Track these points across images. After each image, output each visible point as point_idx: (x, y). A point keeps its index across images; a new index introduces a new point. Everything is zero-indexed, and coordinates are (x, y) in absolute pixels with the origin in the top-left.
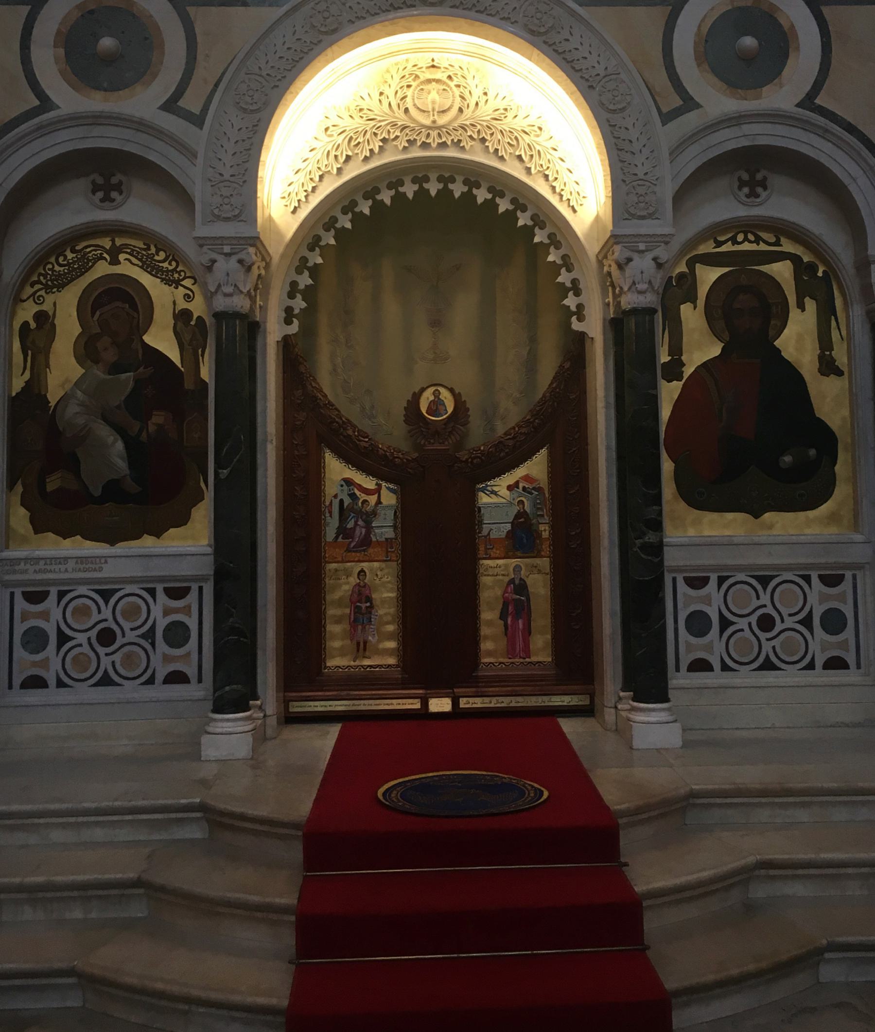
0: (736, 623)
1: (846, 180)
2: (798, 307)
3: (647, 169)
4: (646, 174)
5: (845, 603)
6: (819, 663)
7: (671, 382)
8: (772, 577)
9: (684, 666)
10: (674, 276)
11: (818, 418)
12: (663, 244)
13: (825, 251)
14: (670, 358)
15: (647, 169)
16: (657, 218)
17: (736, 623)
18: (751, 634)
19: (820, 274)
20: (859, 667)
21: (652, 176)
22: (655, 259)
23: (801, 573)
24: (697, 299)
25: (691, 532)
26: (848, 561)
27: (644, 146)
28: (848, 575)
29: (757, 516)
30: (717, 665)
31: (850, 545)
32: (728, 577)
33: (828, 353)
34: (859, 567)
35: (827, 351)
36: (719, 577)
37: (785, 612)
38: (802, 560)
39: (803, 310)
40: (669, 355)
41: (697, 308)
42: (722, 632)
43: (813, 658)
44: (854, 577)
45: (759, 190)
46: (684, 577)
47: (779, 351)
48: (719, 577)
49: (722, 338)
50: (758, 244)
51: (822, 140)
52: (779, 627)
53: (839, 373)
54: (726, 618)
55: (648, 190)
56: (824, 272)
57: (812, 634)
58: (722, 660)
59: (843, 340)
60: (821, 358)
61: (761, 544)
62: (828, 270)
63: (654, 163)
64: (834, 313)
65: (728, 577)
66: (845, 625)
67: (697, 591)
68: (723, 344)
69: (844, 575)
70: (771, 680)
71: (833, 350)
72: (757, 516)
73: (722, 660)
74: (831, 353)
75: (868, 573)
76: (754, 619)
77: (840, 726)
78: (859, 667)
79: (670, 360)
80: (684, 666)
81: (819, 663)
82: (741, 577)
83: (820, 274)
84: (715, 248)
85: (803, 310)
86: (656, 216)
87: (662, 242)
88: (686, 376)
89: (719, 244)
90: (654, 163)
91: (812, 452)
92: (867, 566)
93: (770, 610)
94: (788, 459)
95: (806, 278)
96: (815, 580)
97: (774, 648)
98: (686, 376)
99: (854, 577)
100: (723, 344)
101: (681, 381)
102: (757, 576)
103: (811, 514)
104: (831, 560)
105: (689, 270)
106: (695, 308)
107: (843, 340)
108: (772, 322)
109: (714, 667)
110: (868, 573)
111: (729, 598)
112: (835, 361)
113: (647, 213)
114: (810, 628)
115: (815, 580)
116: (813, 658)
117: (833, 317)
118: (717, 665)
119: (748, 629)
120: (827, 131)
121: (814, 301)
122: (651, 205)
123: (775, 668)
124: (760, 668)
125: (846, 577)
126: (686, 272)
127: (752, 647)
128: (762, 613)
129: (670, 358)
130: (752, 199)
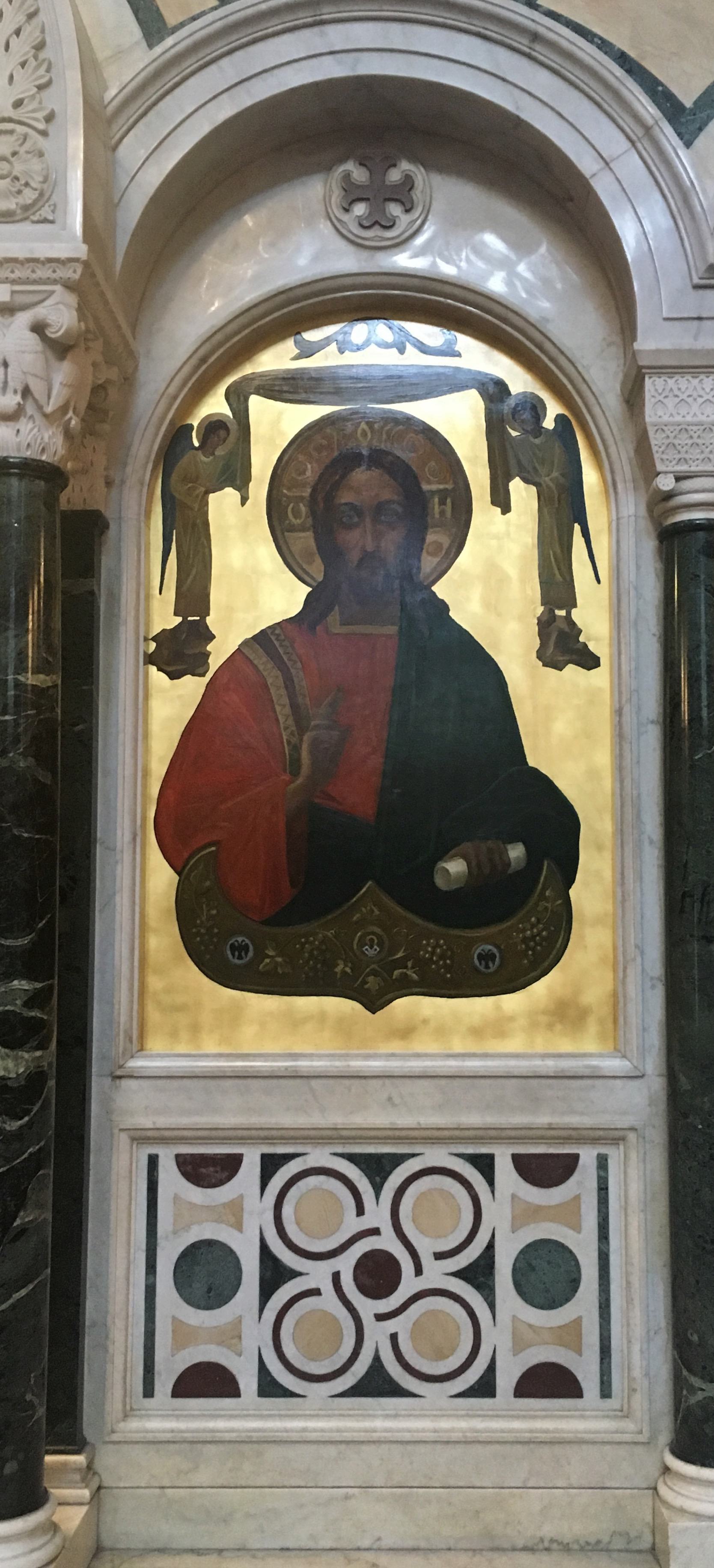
0: (300, 1274)
1: (586, 164)
2: (494, 503)
3: (22, 92)
4: (18, 104)
5: (577, 1228)
6: (506, 1381)
7: (179, 677)
8: (398, 1160)
9: (164, 1383)
10: (195, 424)
11: (535, 772)
12: (58, 288)
13: (552, 359)
14: (179, 619)
15: (22, 92)
16: (45, 221)
17: (300, 1274)
18: (340, 1304)
19: (549, 423)
20: (606, 1392)
21: (34, 111)
22: (39, 328)
23: (470, 1150)
24: (250, 480)
25: (210, 1046)
26: (586, 1121)
27: (18, 32)
28: (588, 1156)
29: (374, 1004)
30: (248, 1382)
31: (589, 1082)
32: (288, 1158)
33: (563, 613)
34: (616, 1138)
35: (561, 608)
36: (263, 1156)
37: (425, 1247)
38: (474, 1119)
39: (506, 508)
40: (176, 614)
41: (248, 503)
42: (266, 1293)
43: (491, 1368)
44: (602, 1163)
45: (395, 209)
46: (178, 1157)
47: (443, 607)
48: (263, 1156)
49: (307, 573)
50: (402, 351)
51: (524, 62)
52: (409, 1285)
53: (590, 661)
54: (275, 1261)
55: (21, 145)
56: (560, 419)
57: (492, 1306)
58: (262, 1368)
59: (599, 581)
60: (545, 624)
61: (365, 1077)
62: (566, 413)
63: (42, 77)
64: (580, 516)
65: (288, 1158)
66: (574, 1283)
67: (209, 1191)
68: (310, 589)
69: (576, 1158)
70: (379, 1424)
71: (575, 606)
72: (374, 1004)
73: (262, 1368)
74: (569, 613)
75: (633, 1156)
76: (346, 1264)
77: (547, 1549)
78: (606, 1392)
79: (180, 624)
80: (164, 1383)
81: (506, 1381)
82: (319, 1157)
83: (549, 423)
84: (297, 358)
85: (506, 508)
86: (46, 212)
87: (55, 282)
88: (215, 663)
89: (307, 351)
90: (42, 77)
91: (516, 852)
92: (632, 1137)
93: (388, 1242)
94: (456, 867)
95: (514, 434)
96: (504, 1168)
97: (394, 1337)
98: (215, 663)
99: (602, 1163)
100: (310, 589)
101: (203, 675)
102: (361, 1155)
103: (511, 1002)
104: (543, 1119)
105: (233, 414)
106: (244, 500)
107: (599, 581)
108: (431, 537)
109: (242, 1386)
110: (633, 1156)
111: (287, 1211)
112: (580, 631)
113: (17, 204)
114: (486, 1289)
115: (504, 1168)
116: (491, 1368)
117: (577, 527)
118: (248, 1382)
119: (333, 1292)
120: (535, 37)
121: (534, 489)
122: (27, 184)
123: (397, 1391)
124: (354, 1391)
125: (581, 1162)
126: (229, 417)
127: (432, 1314)
128: (368, 1249)
129: (179, 619)
130: (376, 232)
